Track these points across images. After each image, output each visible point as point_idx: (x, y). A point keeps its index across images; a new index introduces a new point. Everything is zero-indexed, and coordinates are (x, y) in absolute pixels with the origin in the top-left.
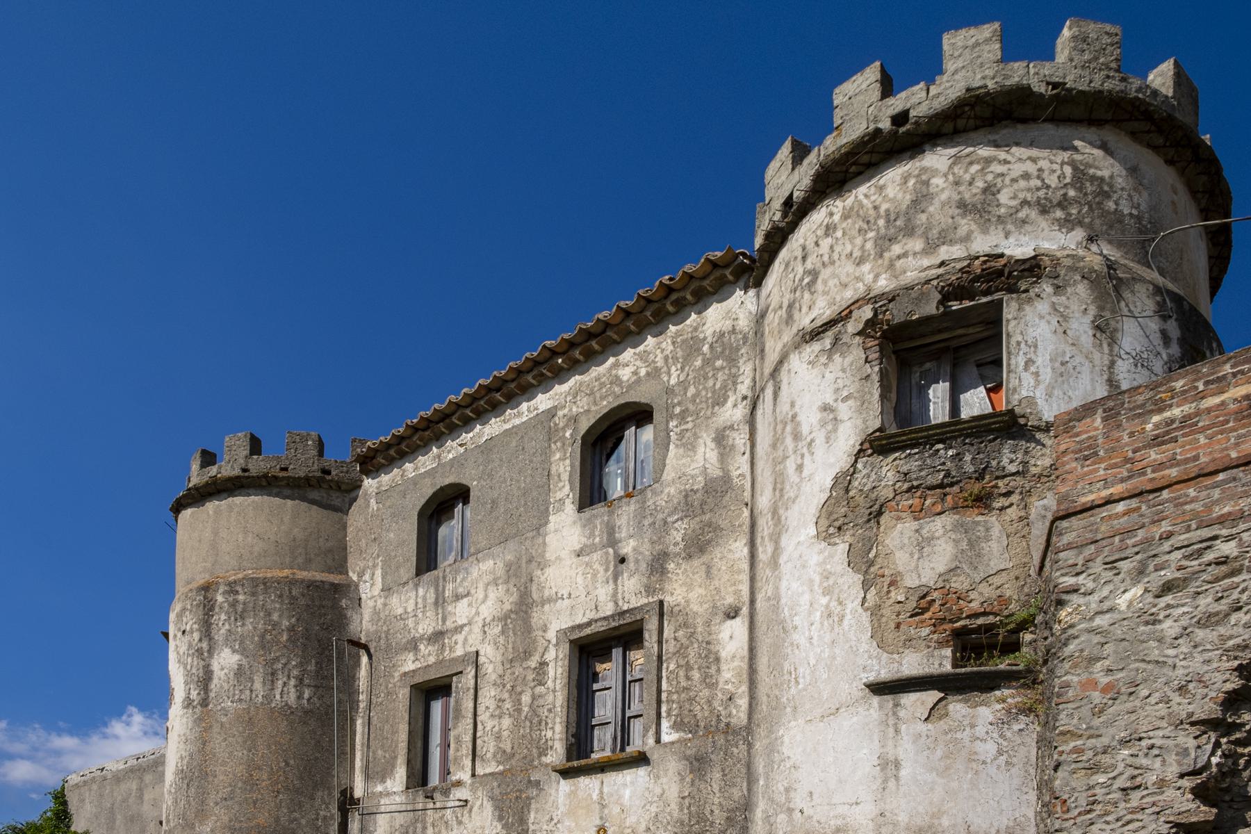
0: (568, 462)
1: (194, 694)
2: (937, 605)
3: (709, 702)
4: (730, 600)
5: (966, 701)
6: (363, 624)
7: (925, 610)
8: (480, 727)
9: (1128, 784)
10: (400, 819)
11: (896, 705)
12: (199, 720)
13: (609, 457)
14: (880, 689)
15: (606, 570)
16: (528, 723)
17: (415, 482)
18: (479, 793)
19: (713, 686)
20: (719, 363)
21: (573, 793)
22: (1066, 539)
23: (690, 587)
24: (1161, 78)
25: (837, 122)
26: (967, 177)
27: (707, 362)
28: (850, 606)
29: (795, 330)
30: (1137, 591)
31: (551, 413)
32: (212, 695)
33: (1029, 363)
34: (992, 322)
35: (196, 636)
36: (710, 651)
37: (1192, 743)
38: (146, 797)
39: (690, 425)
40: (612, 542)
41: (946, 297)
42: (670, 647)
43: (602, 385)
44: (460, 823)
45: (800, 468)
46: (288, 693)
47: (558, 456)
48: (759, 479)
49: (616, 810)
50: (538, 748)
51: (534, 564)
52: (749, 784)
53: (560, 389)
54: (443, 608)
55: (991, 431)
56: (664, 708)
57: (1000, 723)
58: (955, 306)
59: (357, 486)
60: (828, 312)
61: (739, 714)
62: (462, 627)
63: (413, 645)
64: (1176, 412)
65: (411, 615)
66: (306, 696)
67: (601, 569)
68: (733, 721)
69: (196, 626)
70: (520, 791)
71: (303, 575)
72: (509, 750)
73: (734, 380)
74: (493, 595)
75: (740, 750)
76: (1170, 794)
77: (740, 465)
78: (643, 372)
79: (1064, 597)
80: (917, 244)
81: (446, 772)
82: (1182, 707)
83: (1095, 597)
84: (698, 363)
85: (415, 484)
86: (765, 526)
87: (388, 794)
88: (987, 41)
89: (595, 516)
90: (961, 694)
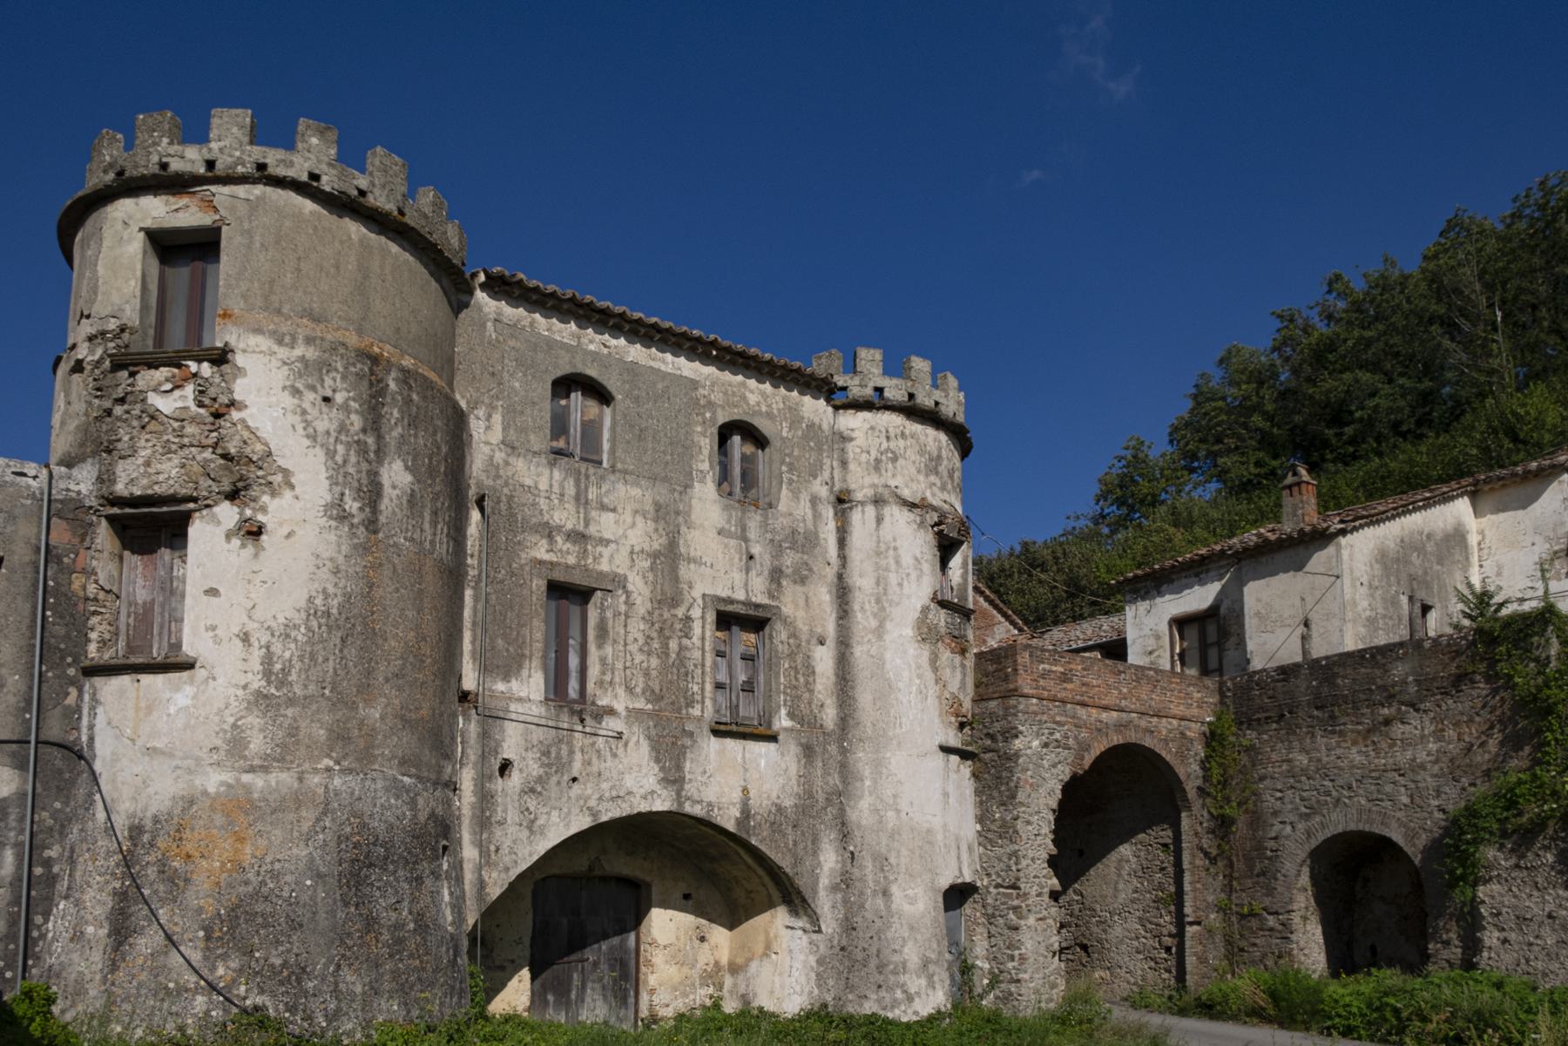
3: (810, 703)
10: (538, 734)
12: (364, 549)
14: (946, 750)
15: (741, 560)
16: (675, 671)
17: (551, 344)
18: (635, 729)
19: (811, 691)
21: (721, 752)
32: (382, 519)
44: (615, 755)
45: (900, 585)
50: (686, 698)
51: (681, 519)
54: (585, 508)
61: (829, 716)
65: (543, 494)
67: (737, 556)
70: (676, 737)
72: (657, 690)
78: (764, 409)
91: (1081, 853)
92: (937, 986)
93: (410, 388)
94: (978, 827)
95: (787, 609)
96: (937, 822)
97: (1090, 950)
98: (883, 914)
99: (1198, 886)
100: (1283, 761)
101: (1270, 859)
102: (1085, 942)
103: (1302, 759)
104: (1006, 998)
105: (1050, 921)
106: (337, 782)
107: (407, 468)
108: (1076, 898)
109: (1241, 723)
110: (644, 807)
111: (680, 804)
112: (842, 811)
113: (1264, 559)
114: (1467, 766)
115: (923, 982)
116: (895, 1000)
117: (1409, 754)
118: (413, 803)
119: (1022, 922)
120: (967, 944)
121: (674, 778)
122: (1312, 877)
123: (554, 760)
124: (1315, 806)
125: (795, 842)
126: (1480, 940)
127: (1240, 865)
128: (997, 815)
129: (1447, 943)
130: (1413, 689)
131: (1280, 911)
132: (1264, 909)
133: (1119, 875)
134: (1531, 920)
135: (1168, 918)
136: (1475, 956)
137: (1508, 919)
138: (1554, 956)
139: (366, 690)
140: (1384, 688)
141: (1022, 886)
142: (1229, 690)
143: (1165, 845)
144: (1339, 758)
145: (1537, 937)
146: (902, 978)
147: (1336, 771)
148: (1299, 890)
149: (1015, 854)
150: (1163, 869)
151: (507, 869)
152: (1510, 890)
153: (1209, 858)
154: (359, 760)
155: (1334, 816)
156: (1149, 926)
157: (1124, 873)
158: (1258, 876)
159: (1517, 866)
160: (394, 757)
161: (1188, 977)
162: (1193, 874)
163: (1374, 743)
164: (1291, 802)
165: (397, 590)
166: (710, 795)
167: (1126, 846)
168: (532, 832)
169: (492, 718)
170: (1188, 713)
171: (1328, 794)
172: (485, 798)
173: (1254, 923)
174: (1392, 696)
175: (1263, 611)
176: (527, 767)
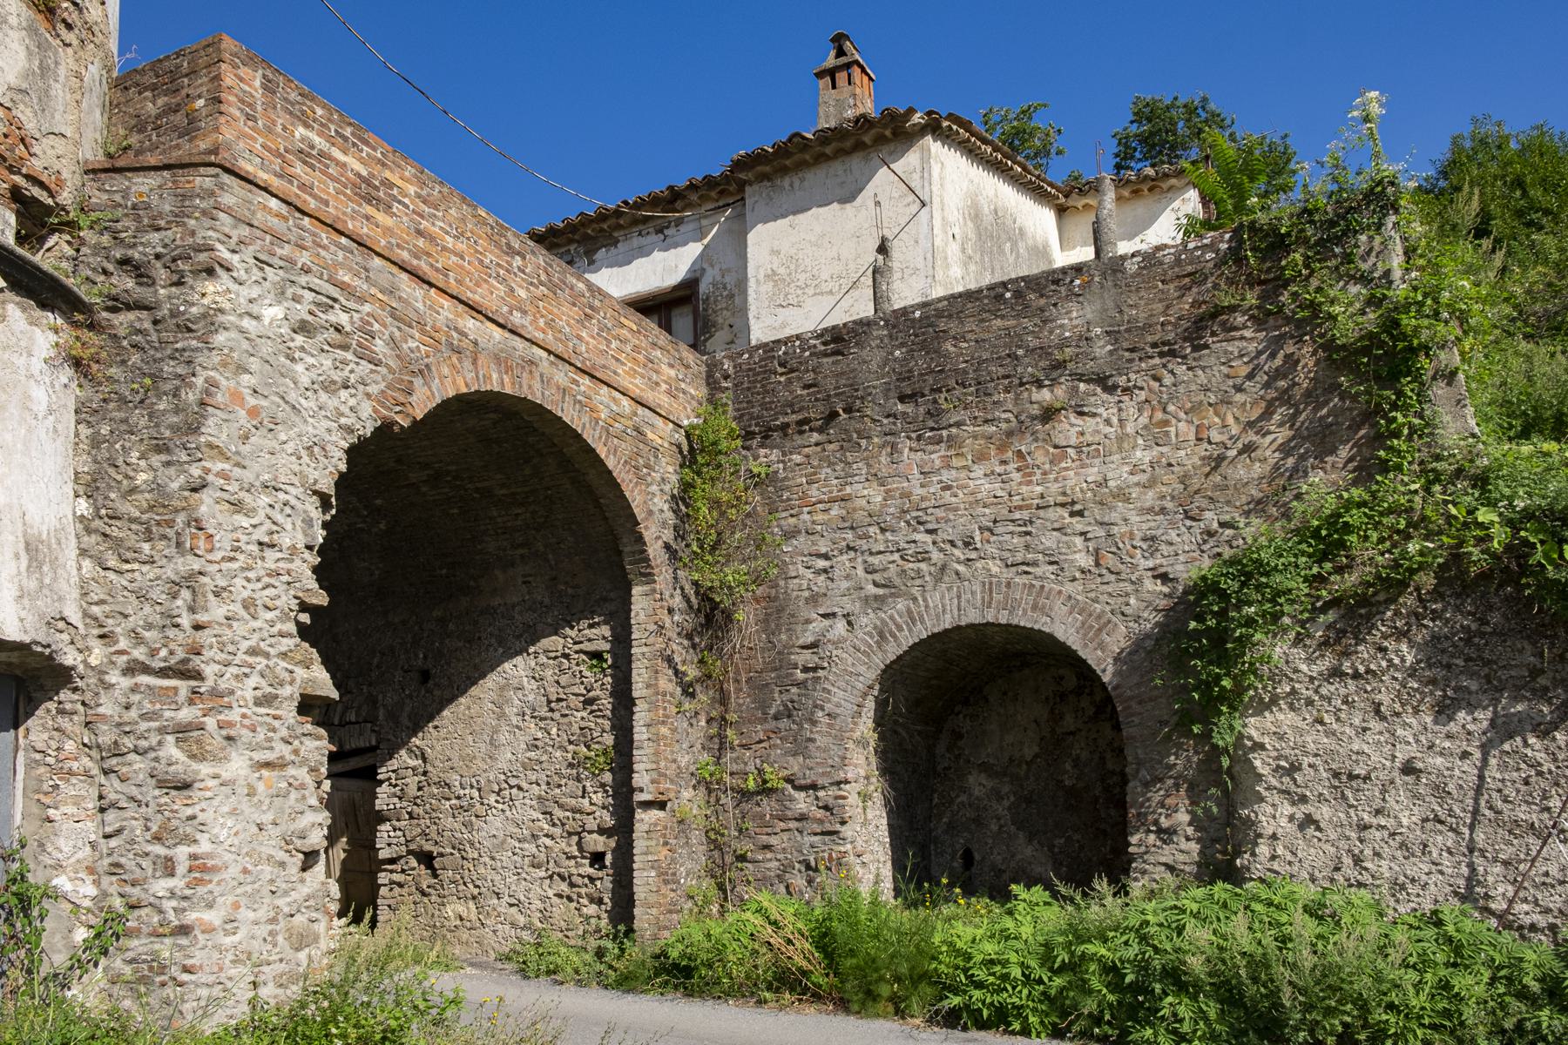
5: (24, 310)
9: (266, 539)
76: (297, 565)
79: (218, 268)
90: (18, 294)
91: (425, 676)
94: (83, 506)
97: (436, 864)
99: (664, 730)
100: (832, 501)
101: (801, 684)
102: (428, 847)
103: (869, 495)
104: (143, 980)
105: (302, 774)
108: (413, 763)
109: (749, 435)
113: (786, 182)
114: (1216, 487)
117: (1093, 474)
119: (205, 769)
120: (30, 830)
122: (879, 722)
124: (897, 581)
126: (1250, 823)
127: (741, 699)
128: (142, 477)
129: (1167, 835)
130: (1102, 349)
131: (820, 782)
132: (788, 780)
133: (502, 716)
134: (1367, 778)
135: (598, 798)
136: (1238, 853)
137: (1314, 780)
138: (1417, 851)
140: (1043, 351)
141: (209, 670)
142: (726, 377)
143: (597, 656)
144: (948, 488)
145: (1378, 812)
147: (940, 513)
148: (858, 742)
149: (190, 581)
150: (589, 702)
152: (1321, 722)
153: (680, 683)
155: (934, 599)
156: (558, 813)
157: (511, 711)
158: (776, 718)
159: (1336, 673)
161: (636, 911)
162: (653, 707)
163: (1019, 453)
164: (847, 577)
167: (519, 660)
170: (649, 396)
171: (923, 557)
173: (767, 806)
174: (1060, 365)
175: (782, 271)
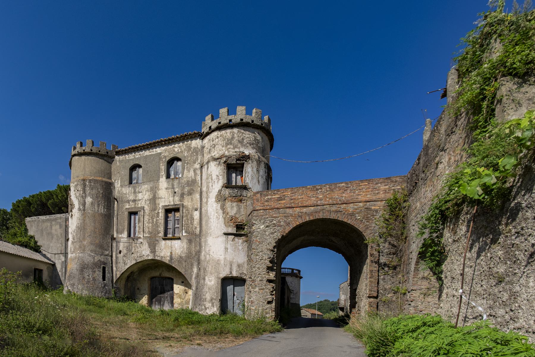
0: (164, 166)
1: (81, 207)
2: (234, 219)
3: (192, 228)
4: (196, 207)
6: (116, 194)
7: (232, 220)
8: (144, 225)
10: (126, 244)
11: (228, 238)
12: (83, 214)
13: (171, 167)
14: (226, 234)
15: (172, 194)
17: (129, 160)
18: (145, 241)
19: (193, 224)
20: (194, 154)
21: (165, 244)
22: (255, 214)
23: (188, 202)
24: (266, 118)
25: (220, 117)
26: (240, 135)
27: (192, 153)
28: (221, 217)
29: (211, 155)
30: (263, 226)
31: (160, 154)
32: (86, 208)
33: (248, 176)
34: (243, 165)
35: (82, 192)
36: (192, 217)
37: (269, 253)
38: (53, 228)
39: (189, 166)
40: (173, 188)
41: (237, 160)
42: (184, 214)
43: (171, 151)
44: (140, 247)
45: (212, 186)
46: (102, 210)
47: (162, 164)
48: (203, 184)
49: (174, 249)
51: (156, 189)
52: (200, 247)
53: (163, 148)
55: (242, 188)
56: (183, 228)
57: (242, 243)
58: (238, 162)
59: (114, 158)
60: (217, 155)
61: (198, 231)
62: (140, 200)
63: (128, 202)
64: (269, 197)
66: (105, 211)
67: (171, 194)
68: (196, 233)
69: (81, 190)
70: (154, 242)
71: (104, 179)
73: (197, 159)
74: (147, 194)
75: (198, 239)
76: (266, 261)
77: (198, 178)
78: (180, 151)
80: (232, 147)
81: (135, 234)
82: (269, 247)
83: (258, 226)
84: (191, 152)
85: (129, 161)
86: (204, 195)
87: (123, 238)
88: (244, 110)
89: (170, 181)
92: (215, 306)
93: (91, 183)
95: (186, 203)
96: (222, 258)
98: (203, 285)
106: (80, 255)
107: (91, 198)
110: (146, 258)
111: (155, 257)
112: (199, 257)
115: (210, 305)
116: (202, 309)
118: (94, 258)
121: (153, 251)
123: (129, 249)
125: (185, 266)
139: (84, 239)
146: (205, 303)
151: (120, 272)
154: (83, 251)
160: (89, 250)
165: (89, 220)
166: (162, 254)
168: (125, 264)
169: (118, 242)
172: (117, 258)
176: (124, 251)
